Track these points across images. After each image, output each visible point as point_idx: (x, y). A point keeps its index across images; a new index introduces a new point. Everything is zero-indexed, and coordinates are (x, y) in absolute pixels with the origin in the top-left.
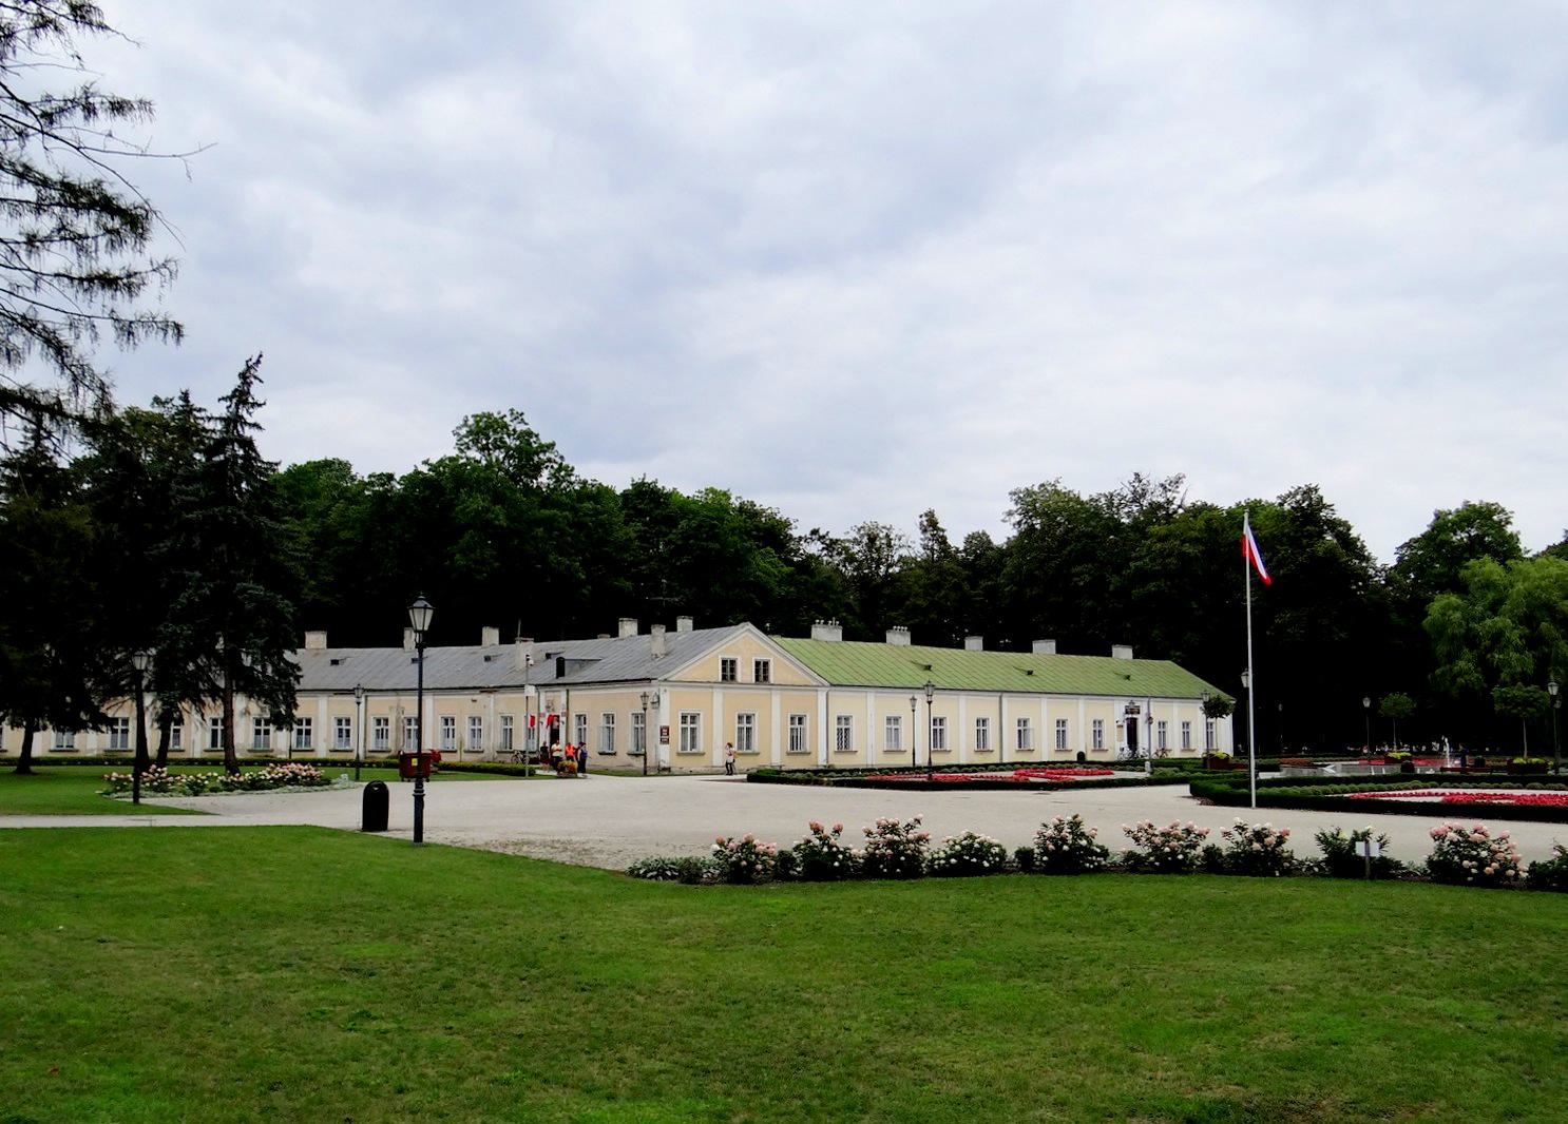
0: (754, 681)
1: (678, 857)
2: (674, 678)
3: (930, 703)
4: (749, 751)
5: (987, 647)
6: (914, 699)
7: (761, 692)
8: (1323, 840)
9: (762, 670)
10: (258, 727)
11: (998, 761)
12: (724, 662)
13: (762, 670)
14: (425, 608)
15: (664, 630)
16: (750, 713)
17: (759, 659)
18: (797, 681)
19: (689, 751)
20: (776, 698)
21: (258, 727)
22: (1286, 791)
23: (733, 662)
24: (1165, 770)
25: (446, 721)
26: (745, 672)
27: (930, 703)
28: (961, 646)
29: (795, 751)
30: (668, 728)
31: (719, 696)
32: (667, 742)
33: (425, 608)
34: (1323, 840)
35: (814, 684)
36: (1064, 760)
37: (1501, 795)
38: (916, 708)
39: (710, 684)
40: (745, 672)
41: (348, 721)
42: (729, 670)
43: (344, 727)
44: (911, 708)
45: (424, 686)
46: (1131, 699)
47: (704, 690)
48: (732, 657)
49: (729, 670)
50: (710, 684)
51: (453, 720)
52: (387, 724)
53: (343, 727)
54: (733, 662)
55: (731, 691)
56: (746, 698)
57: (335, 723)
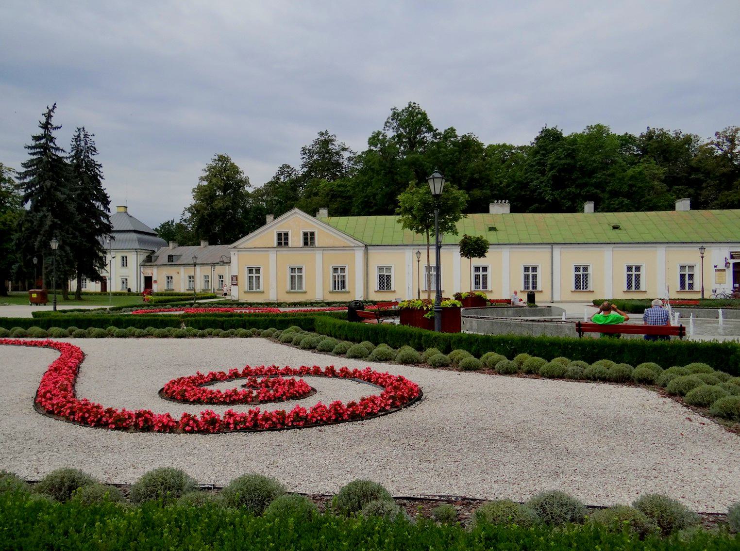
0: (275, 243)
1: (368, 395)
2: (241, 246)
4: (258, 290)
5: (695, 206)
6: (419, 253)
7: (307, 253)
8: (33, 314)
9: (309, 239)
12: (279, 234)
13: (309, 239)
15: (272, 218)
18: (337, 244)
19: (254, 290)
23: (286, 234)
26: (296, 240)
28: (672, 207)
29: (337, 290)
30: (237, 277)
31: (272, 256)
32: (237, 285)
34: (33, 314)
35: (353, 245)
36: (690, 298)
40: (296, 240)
42: (283, 240)
43: (481, 273)
44: (701, 255)
45: (426, 247)
46: (700, 245)
47: (264, 253)
48: (285, 231)
49: (283, 240)
54: (286, 234)
55: (284, 253)
56: (295, 256)
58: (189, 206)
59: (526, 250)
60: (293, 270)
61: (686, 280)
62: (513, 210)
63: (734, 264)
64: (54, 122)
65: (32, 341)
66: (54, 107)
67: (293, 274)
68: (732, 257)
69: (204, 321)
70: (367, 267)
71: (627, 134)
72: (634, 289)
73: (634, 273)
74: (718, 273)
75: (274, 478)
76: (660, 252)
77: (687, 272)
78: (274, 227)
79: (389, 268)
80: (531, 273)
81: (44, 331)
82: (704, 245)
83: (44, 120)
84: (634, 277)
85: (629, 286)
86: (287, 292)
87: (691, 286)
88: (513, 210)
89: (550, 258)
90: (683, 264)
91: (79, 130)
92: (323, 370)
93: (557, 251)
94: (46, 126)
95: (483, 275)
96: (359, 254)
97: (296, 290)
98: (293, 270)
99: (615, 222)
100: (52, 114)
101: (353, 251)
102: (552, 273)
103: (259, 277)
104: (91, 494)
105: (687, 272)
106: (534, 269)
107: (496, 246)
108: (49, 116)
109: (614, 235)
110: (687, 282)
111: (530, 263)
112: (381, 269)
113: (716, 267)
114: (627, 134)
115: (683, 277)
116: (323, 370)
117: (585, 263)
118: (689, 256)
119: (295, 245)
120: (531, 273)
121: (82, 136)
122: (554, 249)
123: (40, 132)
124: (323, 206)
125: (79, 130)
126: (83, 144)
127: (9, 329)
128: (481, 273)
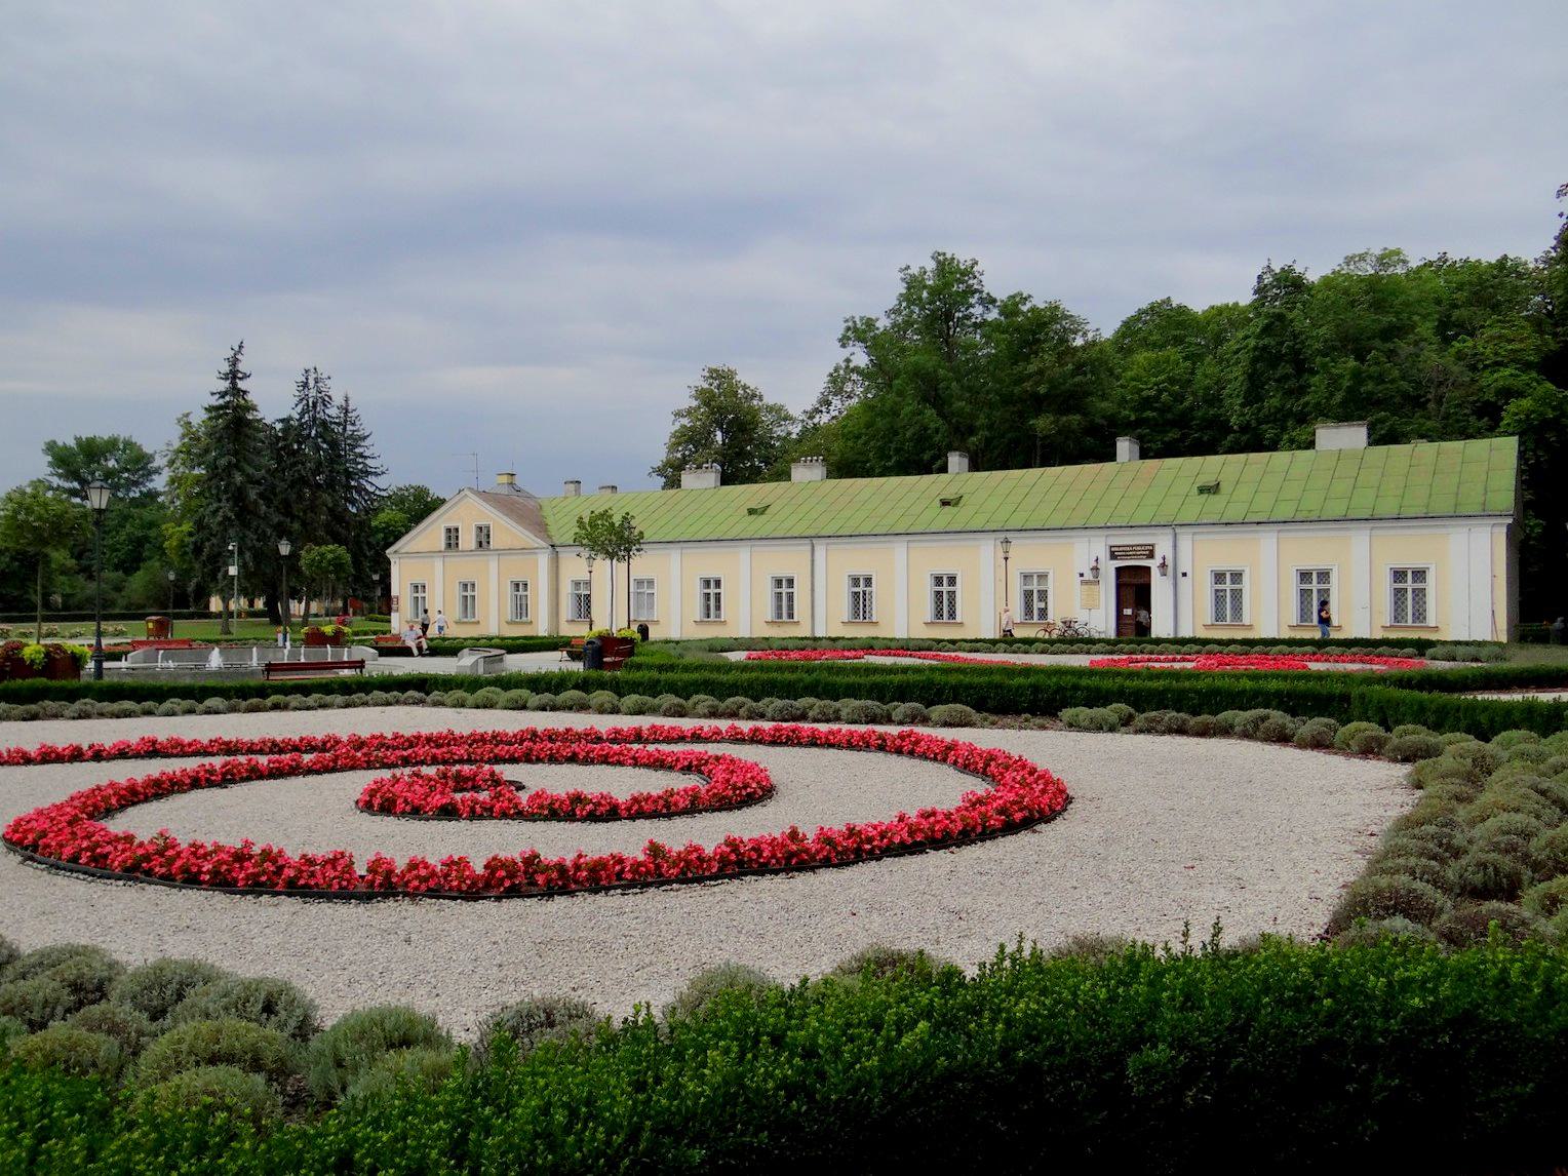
0: (443, 546)
3: (1006, 559)
10: (779, 590)
11: (808, 635)
14: (102, 487)
16: (1236, 568)
17: (480, 523)
20: (493, 564)
21: (779, 590)
22: (1535, 700)
24: (167, 666)
25: (466, 585)
26: (467, 540)
27: (1006, 559)
31: (438, 563)
33: (102, 487)
37: (520, 738)
38: (593, 569)
39: (432, 553)
40: (467, 540)
41: (791, 582)
42: (452, 535)
43: (945, 588)
46: (1002, 535)
50: (432, 553)
51: (473, 585)
52: (526, 590)
53: (712, 598)
55: (454, 560)
56: (466, 567)
57: (1294, 578)
58: (660, 464)
59: (1425, 531)
61: (1034, 601)
62: (1376, 439)
63: (1119, 570)
64: (241, 367)
66: (241, 347)
67: (1306, 586)
68: (1113, 556)
69: (764, 684)
71: (1505, 257)
72: (1410, 623)
73: (1409, 585)
74: (1086, 587)
75: (727, 964)
76: (899, 550)
78: (440, 521)
79: (1043, 577)
80: (784, 590)
81: (682, 701)
82: (1009, 535)
83: (226, 368)
84: (945, 596)
85: (939, 614)
87: (1043, 613)
88: (1376, 439)
89: (810, 563)
90: (1400, 565)
91: (307, 371)
94: (233, 375)
95: (1414, 581)
96: (543, 560)
97: (469, 619)
98: (707, 583)
99: (1208, 479)
100: (238, 357)
101: (534, 556)
102: (813, 590)
105: (1035, 587)
107: (883, 539)
108: (234, 362)
109: (1196, 507)
110: (1037, 605)
112: (1027, 577)
113: (1082, 575)
115: (1028, 595)
118: (789, 560)
120: (1228, 586)
121: (311, 383)
122: (1179, 537)
123: (225, 385)
124: (951, 448)
125: (307, 371)
126: (313, 393)
127: (687, 698)
128: (712, 591)
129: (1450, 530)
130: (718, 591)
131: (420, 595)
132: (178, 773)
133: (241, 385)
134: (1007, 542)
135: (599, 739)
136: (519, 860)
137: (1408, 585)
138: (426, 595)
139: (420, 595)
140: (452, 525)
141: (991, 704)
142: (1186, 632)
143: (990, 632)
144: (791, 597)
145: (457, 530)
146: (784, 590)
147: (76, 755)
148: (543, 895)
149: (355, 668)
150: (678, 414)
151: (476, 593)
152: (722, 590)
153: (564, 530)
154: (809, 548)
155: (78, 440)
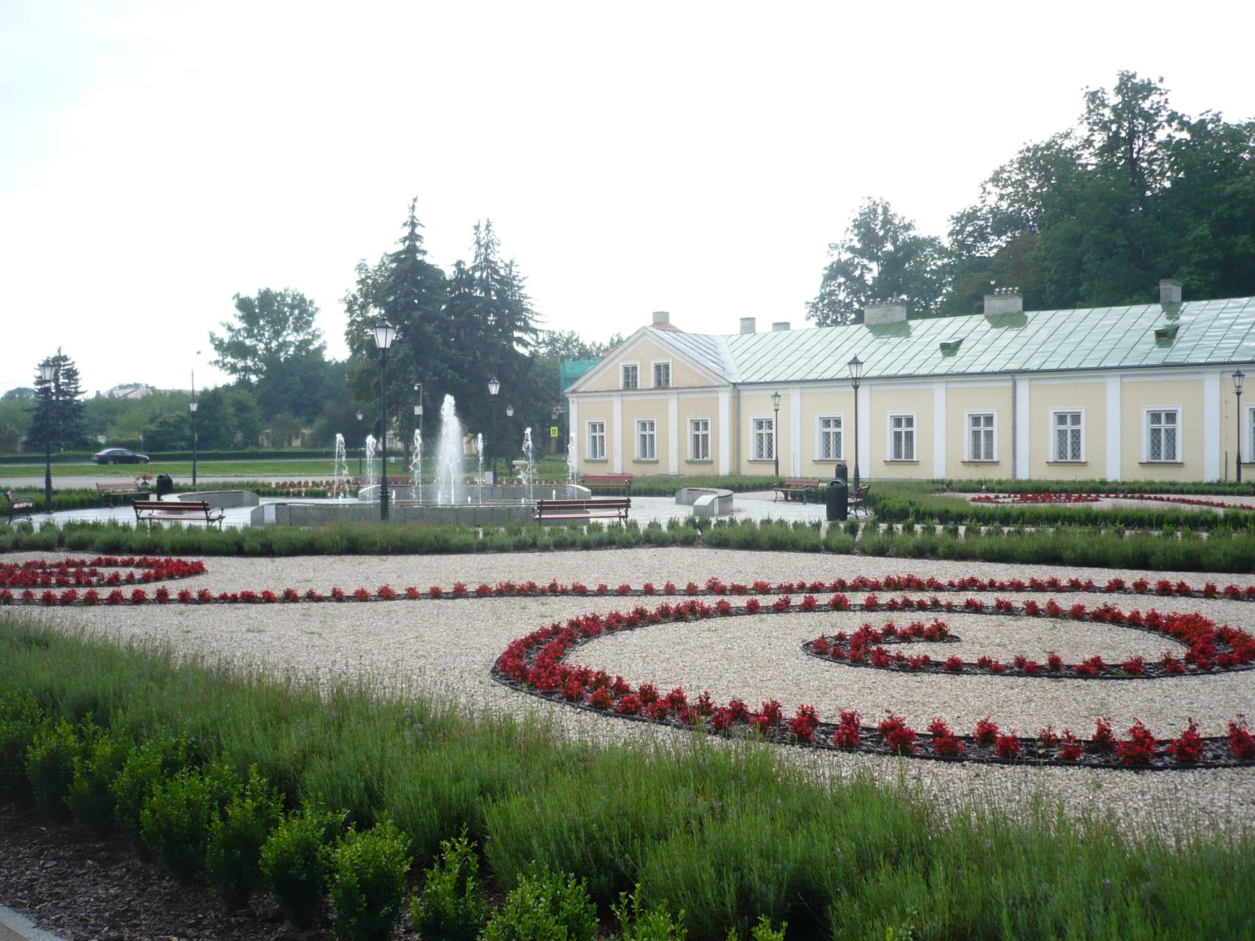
3: (1238, 394)
7: (660, 396)
10: (976, 428)
20: (673, 403)
26: (646, 378)
27: (1238, 394)
31: (617, 403)
38: (1243, 389)
39: (612, 391)
40: (646, 378)
42: (630, 375)
50: (612, 391)
51: (602, 426)
55: (632, 398)
56: (645, 404)
60: (898, 421)
65: (1035, 500)
70: (739, 415)
73: (1163, 425)
77: (904, 429)
86: (635, 462)
92: (195, 595)
93: (1023, 386)
95: (1072, 431)
97: (648, 458)
98: (898, 421)
101: (715, 395)
102: (1014, 428)
103: (1079, 431)
104: (163, 718)
106: (1171, 417)
111: (1163, 407)
114: (1094, 98)
116: (195, 595)
117: (987, 412)
119: (645, 386)
122: (1018, 383)
129: (1205, 376)
130: (838, 430)
131: (648, 432)
132: (581, 618)
133: (418, 231)
134: (777, 395)
135: (939, 588)
136: (324, 695)
137: (1162, 428)
138: (604, 434)
139: (598, 434)
140: (630, 363)
141: (893, 550)
142: (1023, 474)
143: (1212, 474)
144: (989, 434)
145: (667, 367)
146: (982, 428)
147: (530, 591)
148: (995, 761)
149: (619, 507)
150: (833, 247)
151: (655, 433)
152: (915, 429)
153: (818, 359)
154: (1010, 384)
155: (509, 266)
